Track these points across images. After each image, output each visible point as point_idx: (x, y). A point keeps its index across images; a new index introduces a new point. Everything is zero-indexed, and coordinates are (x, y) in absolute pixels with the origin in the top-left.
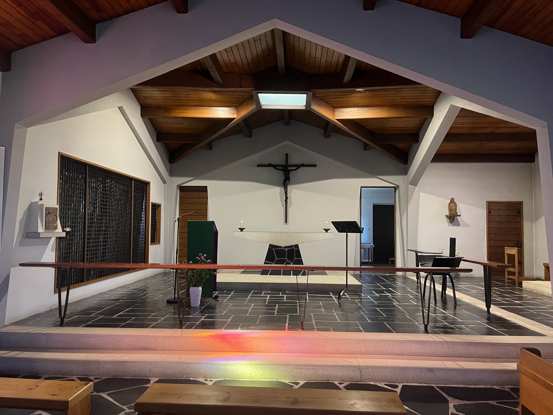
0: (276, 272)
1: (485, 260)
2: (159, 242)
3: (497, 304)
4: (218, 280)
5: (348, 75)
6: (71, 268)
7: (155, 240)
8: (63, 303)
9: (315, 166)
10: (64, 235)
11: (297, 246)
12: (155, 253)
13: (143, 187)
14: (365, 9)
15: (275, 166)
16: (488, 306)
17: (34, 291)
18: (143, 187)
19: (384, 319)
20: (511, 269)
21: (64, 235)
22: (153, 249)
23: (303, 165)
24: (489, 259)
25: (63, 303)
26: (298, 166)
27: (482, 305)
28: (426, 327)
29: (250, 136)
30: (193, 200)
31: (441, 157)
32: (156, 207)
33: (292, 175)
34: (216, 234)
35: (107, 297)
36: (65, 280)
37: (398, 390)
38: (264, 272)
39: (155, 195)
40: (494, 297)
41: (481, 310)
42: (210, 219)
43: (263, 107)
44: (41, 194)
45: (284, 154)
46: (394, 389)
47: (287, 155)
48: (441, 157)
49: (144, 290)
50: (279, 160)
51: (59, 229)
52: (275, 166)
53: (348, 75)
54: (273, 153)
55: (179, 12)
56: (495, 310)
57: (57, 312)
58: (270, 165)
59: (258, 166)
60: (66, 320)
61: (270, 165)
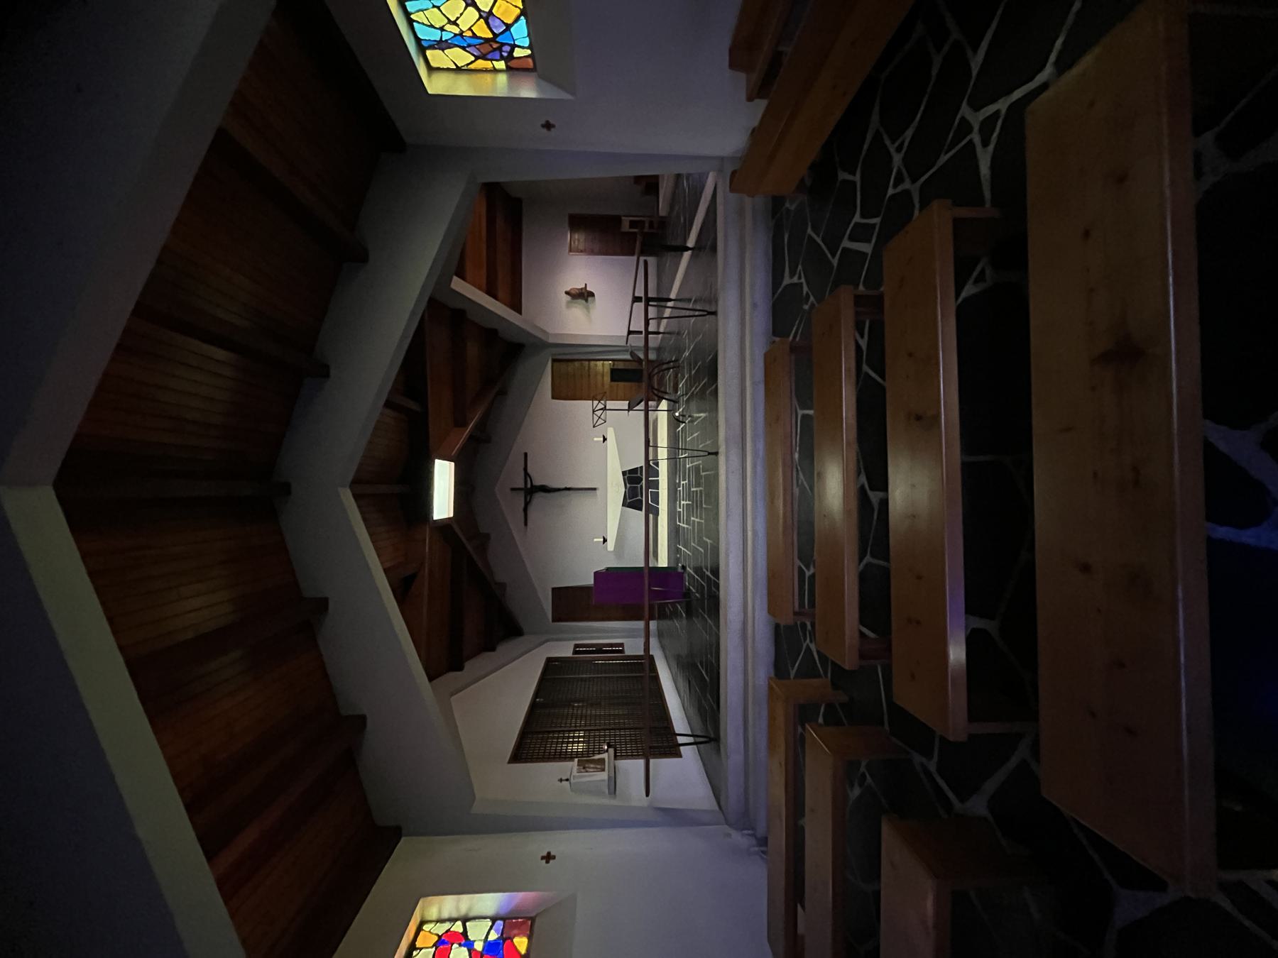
0: (656, 498)
1: (635, 258)
2: (622, 645)
3: (685, 241)
4: (666, 565)
5: (413, 406)
6: (678, 176)
9: (526, 455)
10: (611, 750)
11: (624, 473)
12: (634, 647)
13: (552, 665)
14: (327, 375)
16: (687, 249)
17: (682, 776)
18: (552, 665)
19: (706, 374)
24: (633, 254)
26: (526, 474)
27: (687, 255)
30: (571, 604)
32: (575, 652)
33: (537, 482)
37: (777, 339)
38: (653, 511)
39: (565, 650)
40: (678, 243)
41: (692, 256)
42: (591, 581)
43: (452, 515)
44: (561, 780)
45: (512, 490)
50: (520, 500)
51: (605, 756)
53: (413, 406)
54: (511, 507)
55: (326, 608)
58: (525, 510)
59: (526, 524)
61: (525, 510)
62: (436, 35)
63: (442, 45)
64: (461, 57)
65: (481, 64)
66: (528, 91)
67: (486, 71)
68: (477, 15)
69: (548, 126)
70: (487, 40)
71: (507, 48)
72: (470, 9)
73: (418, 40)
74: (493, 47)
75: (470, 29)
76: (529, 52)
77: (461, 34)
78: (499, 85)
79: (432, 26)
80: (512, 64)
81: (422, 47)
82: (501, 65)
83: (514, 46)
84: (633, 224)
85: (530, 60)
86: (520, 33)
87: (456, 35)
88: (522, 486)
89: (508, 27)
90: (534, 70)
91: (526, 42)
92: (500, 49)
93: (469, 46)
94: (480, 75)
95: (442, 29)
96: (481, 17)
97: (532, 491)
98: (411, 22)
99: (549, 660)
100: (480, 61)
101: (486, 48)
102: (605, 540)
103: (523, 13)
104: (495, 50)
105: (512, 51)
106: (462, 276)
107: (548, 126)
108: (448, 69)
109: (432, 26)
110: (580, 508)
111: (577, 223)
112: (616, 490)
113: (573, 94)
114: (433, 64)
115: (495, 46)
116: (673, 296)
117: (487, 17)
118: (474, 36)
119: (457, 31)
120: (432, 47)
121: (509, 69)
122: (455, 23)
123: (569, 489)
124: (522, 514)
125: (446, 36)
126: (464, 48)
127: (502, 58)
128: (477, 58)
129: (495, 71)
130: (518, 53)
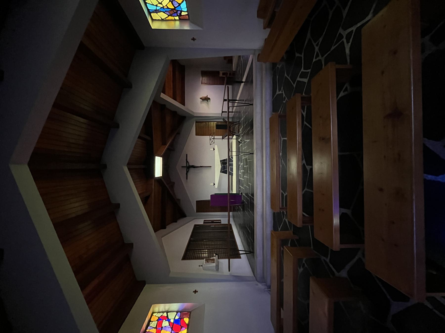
0: (232, 169)
3: (242, 79)
5: (148, 138)
7: (219, 222)
8: (244, 252)
10: (217, 256)
11: (221, 161)
12: (224, 221)
13: (196, 227)
15: (187, 172)
16: (243, 82)
18: (196, 227)
20: (228, 74)
21: (217, 256)
22: (223, 223)
23: (187, 160)
25: (244, 252)
26: (187, 162)
28: (250, 105)
29: (174, 183)
30: (203, 206)
31: (183, 104)
33: (191, 164)
34: (216, 194)
35: (243, 238)
36: (236, 254)
38: (231, 174)
39: (201, 222)
40: (240, 80)
42: (209, 198)
43: (161, 176)
46: (309, 171)
47: (182, 167)
48: (183, 104)
49: (240, 225)
51: (215, 258)
52: (187, 172)
53: (148, 138)
56: (244, 80)
57: (248, 254)
58: (187, 174)
59: (187, 179)
60: (252, 251)
61: (187, 174)
88: (185, 165)
97: (189, 167)
99: (195, 225)
102: (214, 184)
110: (206, 173)
112: (218, 167)
123: (201, 167)
124: (186, 175)
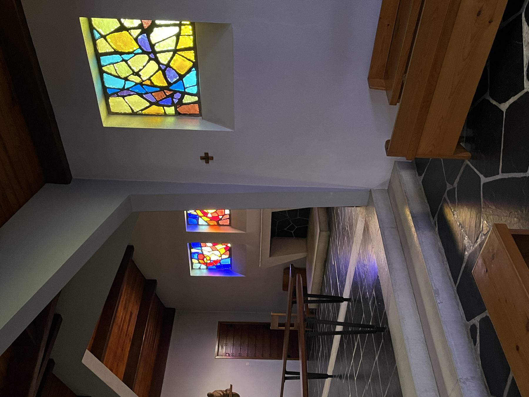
1: (282, 361)
3: (326, 370)
16: (342, 300)
27: (328, 381)
62: (119, 84)
63: (122, 93)
64: (137, 102)
65: (154, 109)
66: (192, 125)
67: (158, 115)
68: (156, 67)
69: (207, 158)
70: (162, 89)
71: (178, 96)
72: (152, 62)
73: (96, 50)
74: (168, 94)
75: (149, 79)
76: (196, 99)
77: (141, 84)
78: (166, 120)
79: (119, 77)
80: (181, 109)
81: (107, 94)
82: (171, 110)
83: (184, 94)
84: (280, 325)
85: (196, 106)
86: (190, 81)
87: (137, 84)
89: (181, 77)
90: (200, 115)
91: (194, 90)
92: (172, 96)
93: (147, 93)
94: (151, 118)
95: (126, 79)
96: (160, 68)
98: (101, 72)
100: (154, 107)
101: (160, 96)
103: (195, 65)
104: (167, 96)
105: (182, 97)
106: (98, 352)
107: (207, 158)
108: (125, 114)
109: (119, 77)
111: (228, 331)
113: (232, 127)
114: (113, 110)
115: (168, 93)
116: (330, 373)
117: (165, 69)
118: (153, 85)
119: (137, 79)
120: (113, 95)
121: (178, 114)
122: (137, 74)
125: (128, 85)
126: (141, 95)
127: (173, 104)
128: (152, 104)
129: (165, 115)
130: (187, 99)
